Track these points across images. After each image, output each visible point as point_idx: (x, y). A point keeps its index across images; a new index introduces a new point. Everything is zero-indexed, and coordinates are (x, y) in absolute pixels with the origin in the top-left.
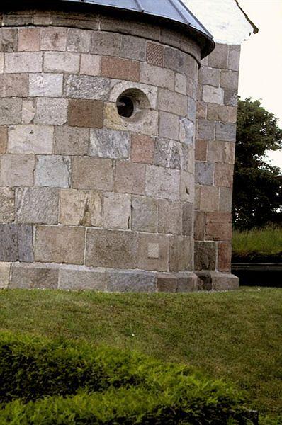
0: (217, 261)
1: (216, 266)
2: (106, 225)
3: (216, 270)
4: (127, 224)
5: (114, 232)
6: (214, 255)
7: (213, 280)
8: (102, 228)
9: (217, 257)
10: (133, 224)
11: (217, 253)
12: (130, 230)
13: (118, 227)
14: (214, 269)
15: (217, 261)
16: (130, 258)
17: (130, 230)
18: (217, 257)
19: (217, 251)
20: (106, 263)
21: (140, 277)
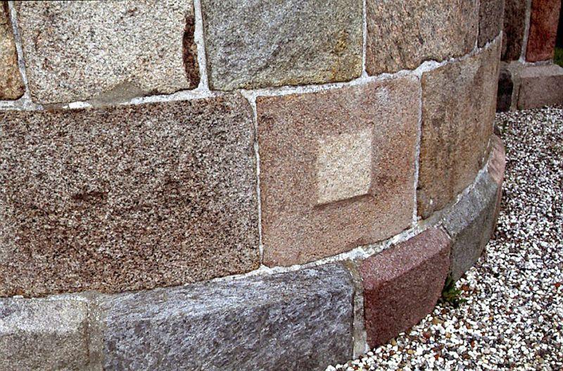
0: (525, 38)
1: (523, 49)
2: (46, 84)
3: (521, 59)
4: (179, 63)
5: (106, 115)
6: (521, 25)
7: (516, 87)
8: (27, 104)
9: (527, 28)
10: (219, 54)
11: (527, 21)
12: (202, 92)
13: (128, 87)
14: (516, 58)
15: (525, 38)
16: (222, 231)
17: (202, 92)
18: (527, 28)
19: (528, 14)
20: (88, 276)
21: (275, 315)
